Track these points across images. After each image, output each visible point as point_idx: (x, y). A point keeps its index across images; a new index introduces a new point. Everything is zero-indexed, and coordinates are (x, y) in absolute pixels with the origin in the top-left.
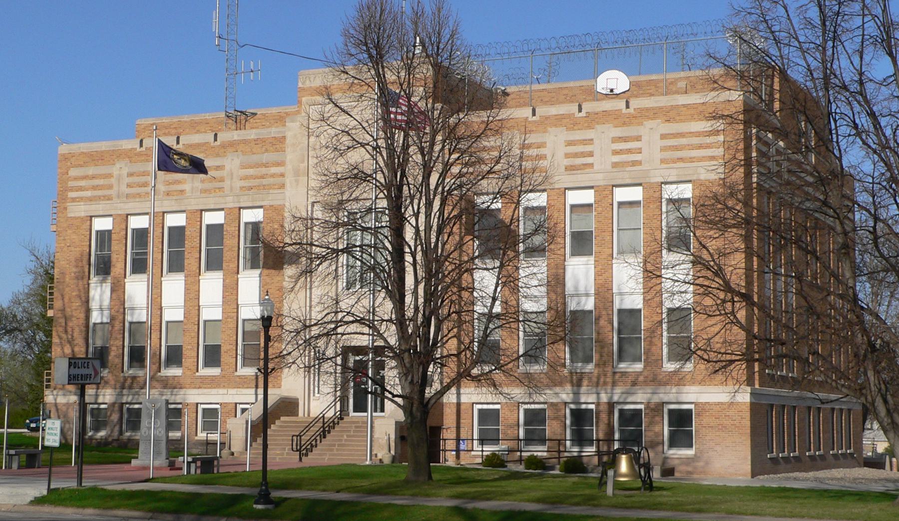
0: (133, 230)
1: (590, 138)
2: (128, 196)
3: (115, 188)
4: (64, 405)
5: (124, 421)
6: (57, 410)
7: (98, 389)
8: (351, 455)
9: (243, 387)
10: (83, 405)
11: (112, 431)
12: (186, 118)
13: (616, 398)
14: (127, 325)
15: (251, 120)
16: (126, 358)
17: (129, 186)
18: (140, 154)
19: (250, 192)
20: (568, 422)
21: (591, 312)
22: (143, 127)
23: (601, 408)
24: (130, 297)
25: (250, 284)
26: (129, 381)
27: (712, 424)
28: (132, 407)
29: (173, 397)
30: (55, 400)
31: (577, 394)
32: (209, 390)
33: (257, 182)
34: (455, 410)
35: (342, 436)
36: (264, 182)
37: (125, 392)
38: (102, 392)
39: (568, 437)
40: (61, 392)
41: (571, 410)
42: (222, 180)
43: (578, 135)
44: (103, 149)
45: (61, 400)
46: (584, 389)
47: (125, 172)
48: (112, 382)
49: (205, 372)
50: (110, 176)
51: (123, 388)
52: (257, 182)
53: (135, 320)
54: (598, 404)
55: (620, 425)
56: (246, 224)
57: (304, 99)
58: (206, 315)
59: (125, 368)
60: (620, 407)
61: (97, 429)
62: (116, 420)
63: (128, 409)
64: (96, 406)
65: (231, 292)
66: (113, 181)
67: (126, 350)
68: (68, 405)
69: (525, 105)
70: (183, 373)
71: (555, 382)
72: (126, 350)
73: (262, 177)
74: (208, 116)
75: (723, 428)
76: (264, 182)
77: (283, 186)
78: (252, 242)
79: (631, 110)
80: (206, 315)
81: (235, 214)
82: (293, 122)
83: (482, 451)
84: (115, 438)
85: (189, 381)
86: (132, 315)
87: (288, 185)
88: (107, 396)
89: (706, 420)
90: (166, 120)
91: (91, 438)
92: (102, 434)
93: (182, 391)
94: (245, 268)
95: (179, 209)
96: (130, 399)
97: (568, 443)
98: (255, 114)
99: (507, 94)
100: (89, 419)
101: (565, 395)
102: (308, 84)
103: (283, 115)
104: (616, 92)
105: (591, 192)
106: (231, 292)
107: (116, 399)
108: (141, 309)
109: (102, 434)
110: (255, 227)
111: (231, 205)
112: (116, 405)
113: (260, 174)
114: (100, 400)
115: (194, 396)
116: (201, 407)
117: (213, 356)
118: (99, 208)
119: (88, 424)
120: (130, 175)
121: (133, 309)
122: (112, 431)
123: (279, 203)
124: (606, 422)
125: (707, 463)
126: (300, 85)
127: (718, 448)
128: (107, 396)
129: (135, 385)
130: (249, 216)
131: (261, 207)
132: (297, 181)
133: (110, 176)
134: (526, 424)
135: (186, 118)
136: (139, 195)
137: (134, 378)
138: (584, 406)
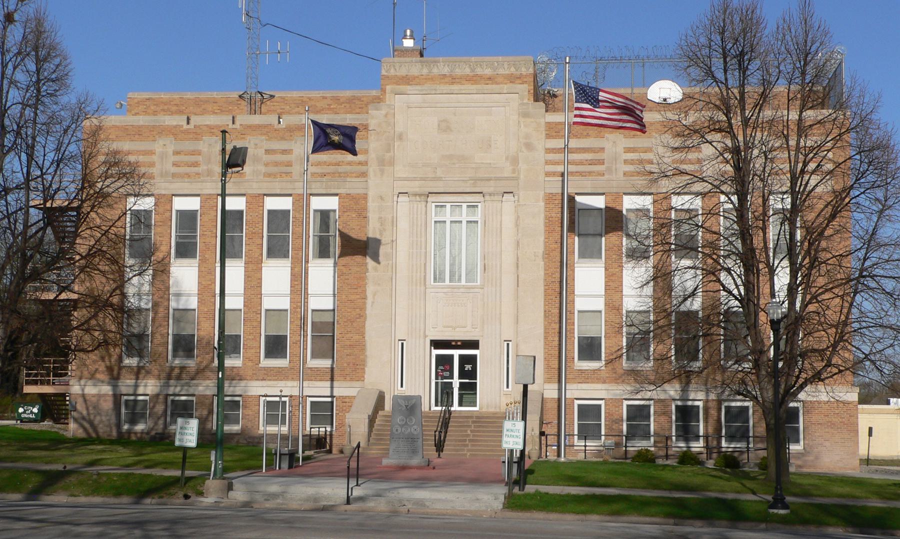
0: (177, 211)
1: (601, 146)
2: (174, 175)
3: (158, 166)
4: (94, 396)
5: (169, 413)
6: (85, 401)
7: (137, 378)
8: (492, 451)
9: (316, 380)
10: (117, 398)
11: (156, 424)
12: (189, 95)
13: (724, 397)
14: (171, 311)
15: (268, 103)
16: (170, 347)
17: (175, 164)
18: (187, 132)
19: (324, 179)
20: (674, 417)
21: (697, 312)
22: (136, 101)
23: (710, 404)
24: (177, 283)
25: (322, 276)
26: (177, 371)
27: (821, 421)
28: (177, 398)
29: (232, 389)
30: (83, 390)
31: (685, 390)
32: (275, 382)
33: (331, 169)
34: (556, 405)
35: (466, 431)
36: (341, 169)
37: (172, 382)
38: (142, 383)
39: (674, 434)
40: (90, 382)
41: (677, 407)
42: (289, 164)
43: (188, 145)
44: (141, 123)
45: (91, 390)
46: (692, 386)
47: (170, 149)
48: (156, 372)
49: (266, 363)
50: (152, 153)
51: (169, 377)
52: (331, 169)
53: (181, 307)
54: (706, 402)
55: (726, 422)
56: (315, 211)
57: (388, 88)
58: (268, 303)
59: (170, 357)
60: (726, 404)
61: (133, 421)
62: (160, 413)
63: (173, 401)
64: (132, 398)
65: (299, 284)
66: (155, 158)
67: (170, 338)
68: (99, 396)
69: (180, 112)
70: (244, 364)
71: (660, 381)
72: (170, 338)
73: (338, 164)
74: (215, 95)
75: (832, 425)
76: (341, 169)
77: (364, 175)
78: (321, 230)
79: (191, 126)
80: (268, 303)
81: (302, 202)
82: (377, 109)
83: (585, 446)
84: (160, 431)
85: (250, 373)
86: (178, 301)
87: (371, 173)
88: (149, 387)
89: (815, 418)
90: (164, 96)
91: (129, 432)
92: (140, 427)
93: (243, 383)
94: (314, 257)
95: (324, 192)
96: (178, 389)
97: (674, 438)
98: (272, 96)
99: (555, 96)
100: (123, 410)
101: (672, 390)
102: (392, 72)
103: (305, 99)
104: (669, 101)
105: (244, 199)
106: (299, 284)
107: (161, 391)
108: (189, 295)
109: (140, 427)
110: (325, 216)
111: (300, 191)
112: (161, 397)
113: (334, 161)
114: (141, 390)
115: (257, 389)
116: (262, 399)
117: (276, 346)
118: (186, 187)
119: (123, 417)
120: (177, 153)
121: (178, 295)
122: (156, 424)
123: (361, 191)
124: (715, 418)
125: (817, 458)
126: (384, 72)
127: (827, 444)
128: (149, 387)
129: (184, 376)
130: (319, 203)
131: (336, 195)
132: (382, 171)
133: (152, 153)
134: (628, 419)
135: (189, 95)
136: (188, 175)
137: (183, 368)
138: (690, 403)
